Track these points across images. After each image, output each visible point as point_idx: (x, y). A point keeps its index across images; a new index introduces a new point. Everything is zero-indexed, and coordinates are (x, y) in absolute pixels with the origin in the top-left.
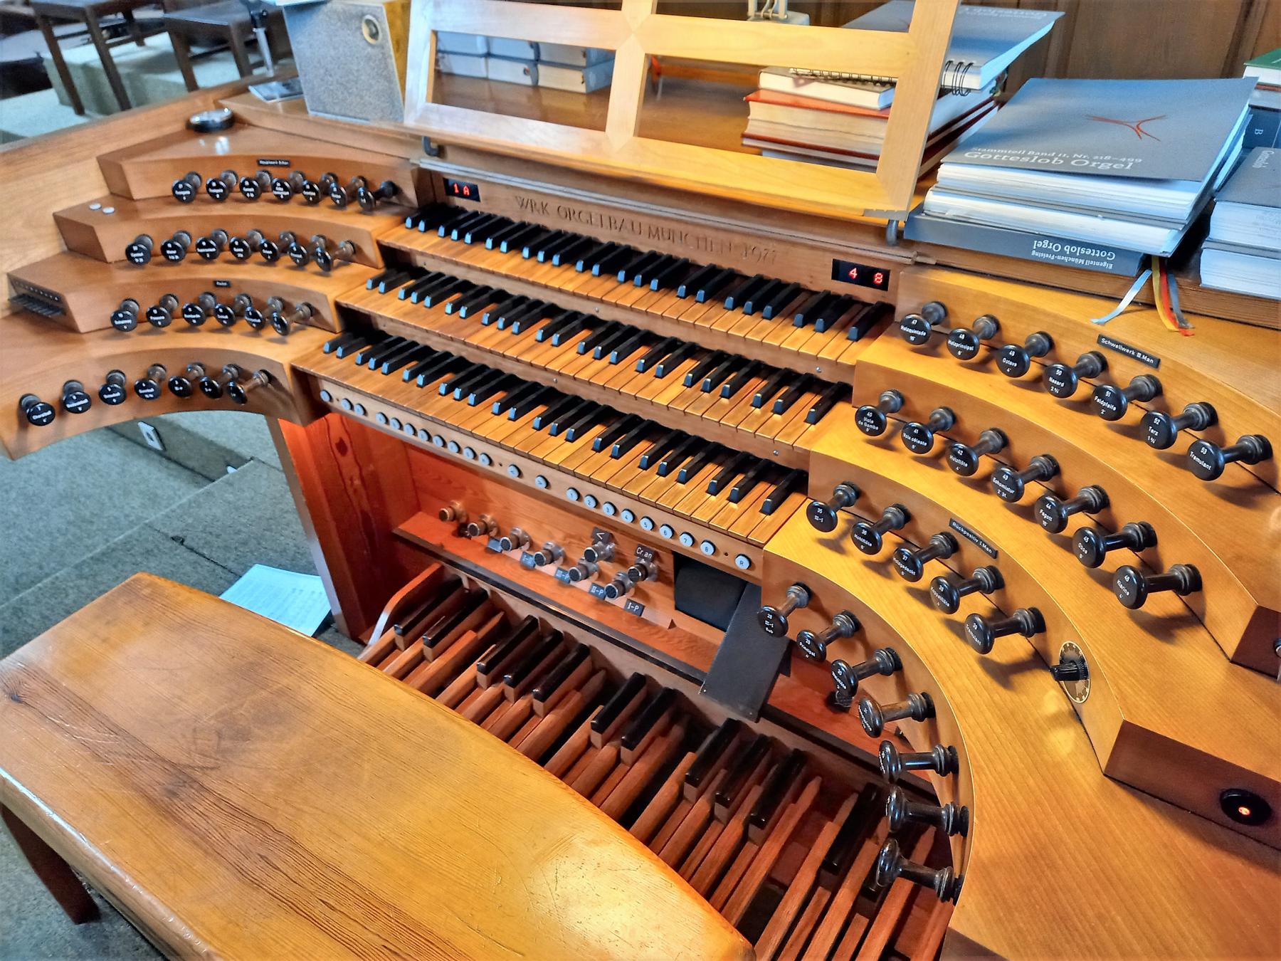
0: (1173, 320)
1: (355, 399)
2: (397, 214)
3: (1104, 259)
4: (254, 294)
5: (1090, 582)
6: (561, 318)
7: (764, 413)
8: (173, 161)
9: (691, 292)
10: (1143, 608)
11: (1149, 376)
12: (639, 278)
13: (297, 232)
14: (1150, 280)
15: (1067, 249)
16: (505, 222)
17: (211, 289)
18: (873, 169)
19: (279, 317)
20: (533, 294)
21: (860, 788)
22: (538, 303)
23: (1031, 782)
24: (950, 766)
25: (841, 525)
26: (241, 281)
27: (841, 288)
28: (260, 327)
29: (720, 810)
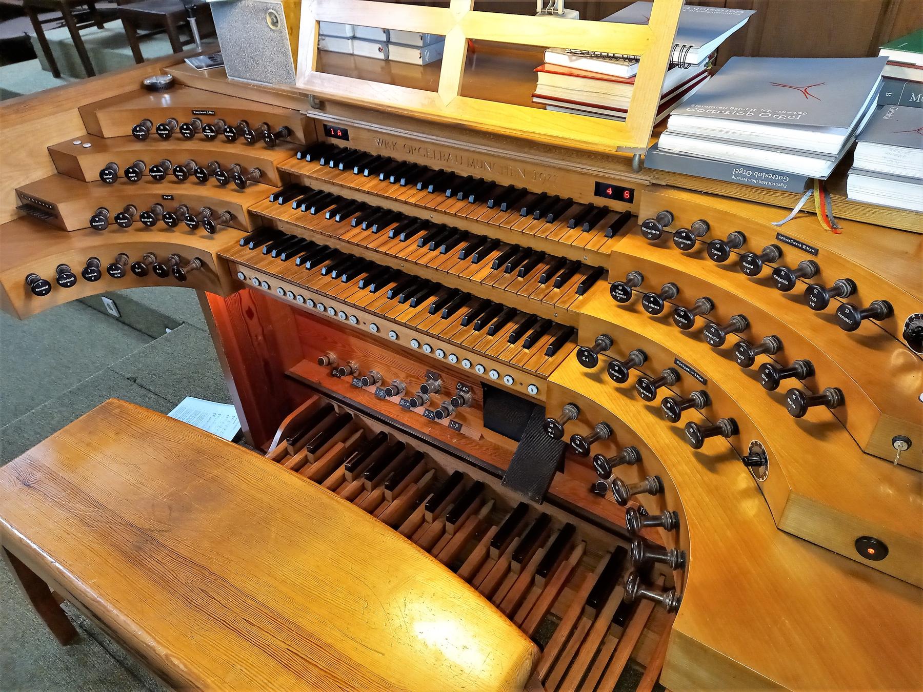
2: (291, 149)
3: (778, 182)
5: (769, 400)
7: (547, 287)
9: (497, 204)
10: (806, 417)
11: (811, 262)
12: (460, 194)
13: (221, 161)
14: (813, 196)
16: (365, 155)
17: (160, 201)
19: (209, 221)
20: (386, 205)
21: (612, 550)
22: (389, 211)
23: (729, 533)
24: (675, 526)
25: (600, 364)
26: (182, 195)
27: (600, 202)
28: (195, 227)
29: (516, 565)
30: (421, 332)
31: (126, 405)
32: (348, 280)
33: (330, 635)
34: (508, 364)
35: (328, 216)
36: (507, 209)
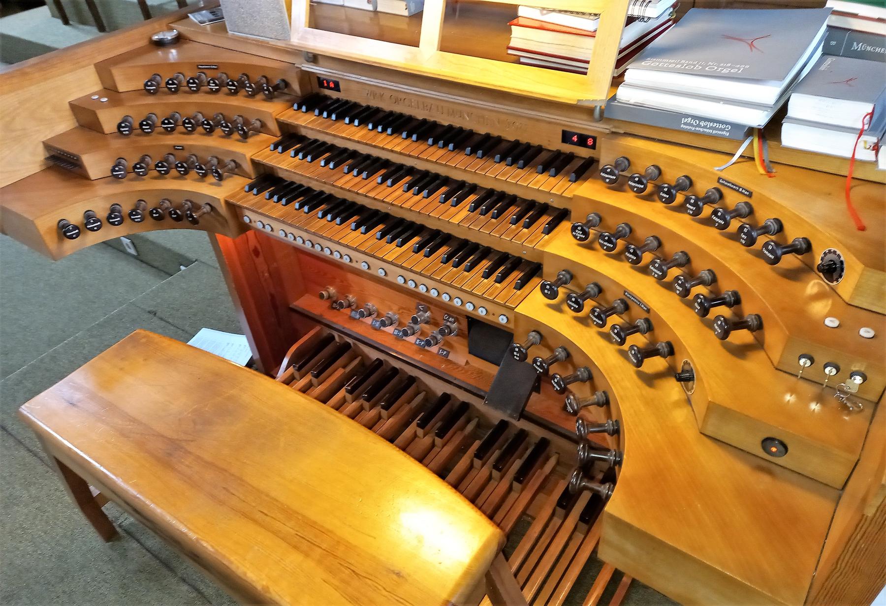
0: (764, 168)
1: (266, 221)
2: (288, 101)
3: (723, 130)
4: (200, 154)
5: (701, 325)
6: (393, 168)
8: (143, 66)
9: (473, 152)
11: (746, 203)
13: (225, 113)
15: (702, 123)
16: (356, 105)
17: (172, 151)
18: (585, 74)
19: (217, 169)
20: (375, 153)
23: (658, 437)
24: (616, 432)
26: (191, 146)
27: (567, 148)
28: (205, 175)
29: (496, 474)
31: (151, 335)
32: (342, 222)
33: (330, 522)
34: (481, 297)
35: (322, 163)
36: (483, 156)
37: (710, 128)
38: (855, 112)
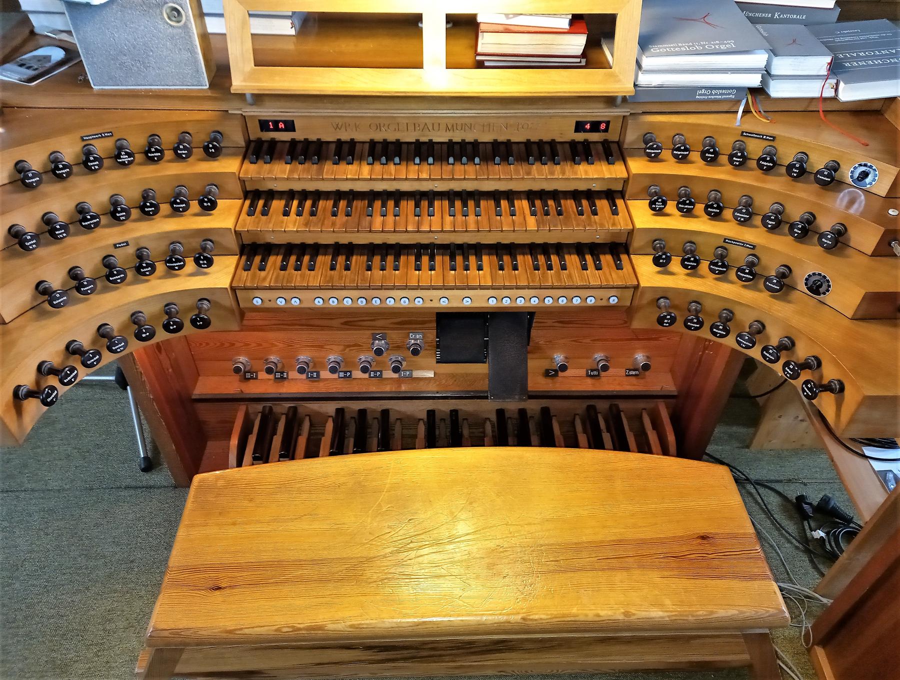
3: (729, 94)
27: (580, 137)
30: (510, 288)
37: (720, 94)
38: (820, 63)
